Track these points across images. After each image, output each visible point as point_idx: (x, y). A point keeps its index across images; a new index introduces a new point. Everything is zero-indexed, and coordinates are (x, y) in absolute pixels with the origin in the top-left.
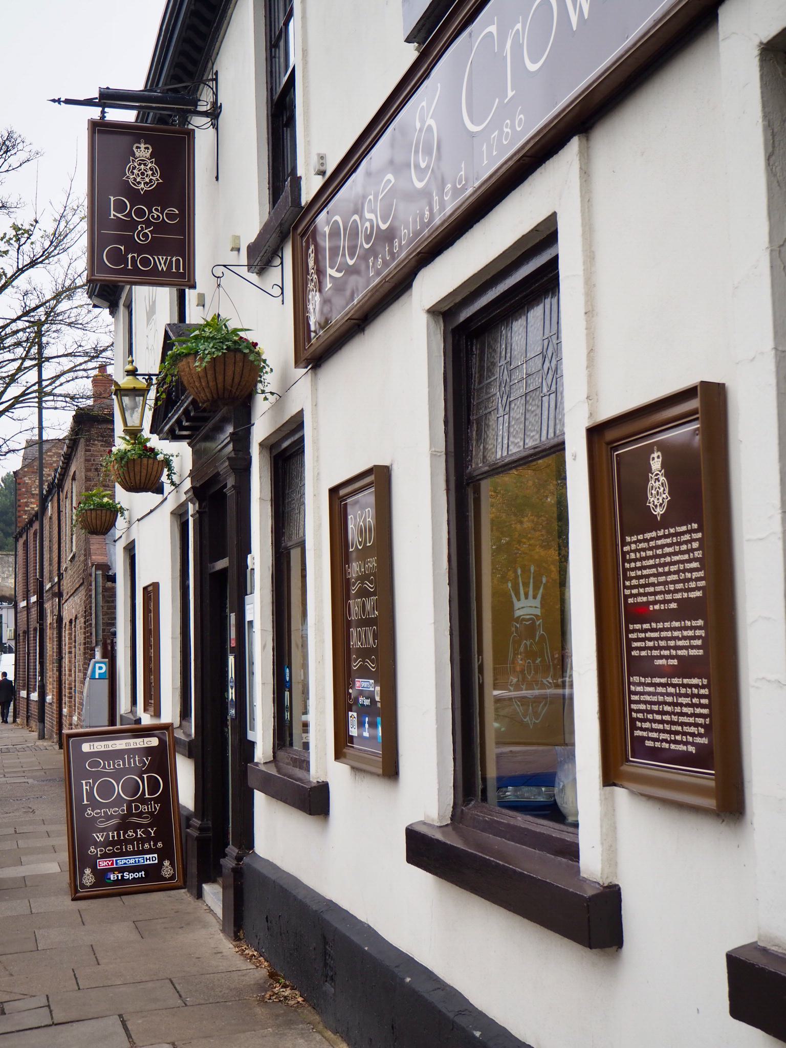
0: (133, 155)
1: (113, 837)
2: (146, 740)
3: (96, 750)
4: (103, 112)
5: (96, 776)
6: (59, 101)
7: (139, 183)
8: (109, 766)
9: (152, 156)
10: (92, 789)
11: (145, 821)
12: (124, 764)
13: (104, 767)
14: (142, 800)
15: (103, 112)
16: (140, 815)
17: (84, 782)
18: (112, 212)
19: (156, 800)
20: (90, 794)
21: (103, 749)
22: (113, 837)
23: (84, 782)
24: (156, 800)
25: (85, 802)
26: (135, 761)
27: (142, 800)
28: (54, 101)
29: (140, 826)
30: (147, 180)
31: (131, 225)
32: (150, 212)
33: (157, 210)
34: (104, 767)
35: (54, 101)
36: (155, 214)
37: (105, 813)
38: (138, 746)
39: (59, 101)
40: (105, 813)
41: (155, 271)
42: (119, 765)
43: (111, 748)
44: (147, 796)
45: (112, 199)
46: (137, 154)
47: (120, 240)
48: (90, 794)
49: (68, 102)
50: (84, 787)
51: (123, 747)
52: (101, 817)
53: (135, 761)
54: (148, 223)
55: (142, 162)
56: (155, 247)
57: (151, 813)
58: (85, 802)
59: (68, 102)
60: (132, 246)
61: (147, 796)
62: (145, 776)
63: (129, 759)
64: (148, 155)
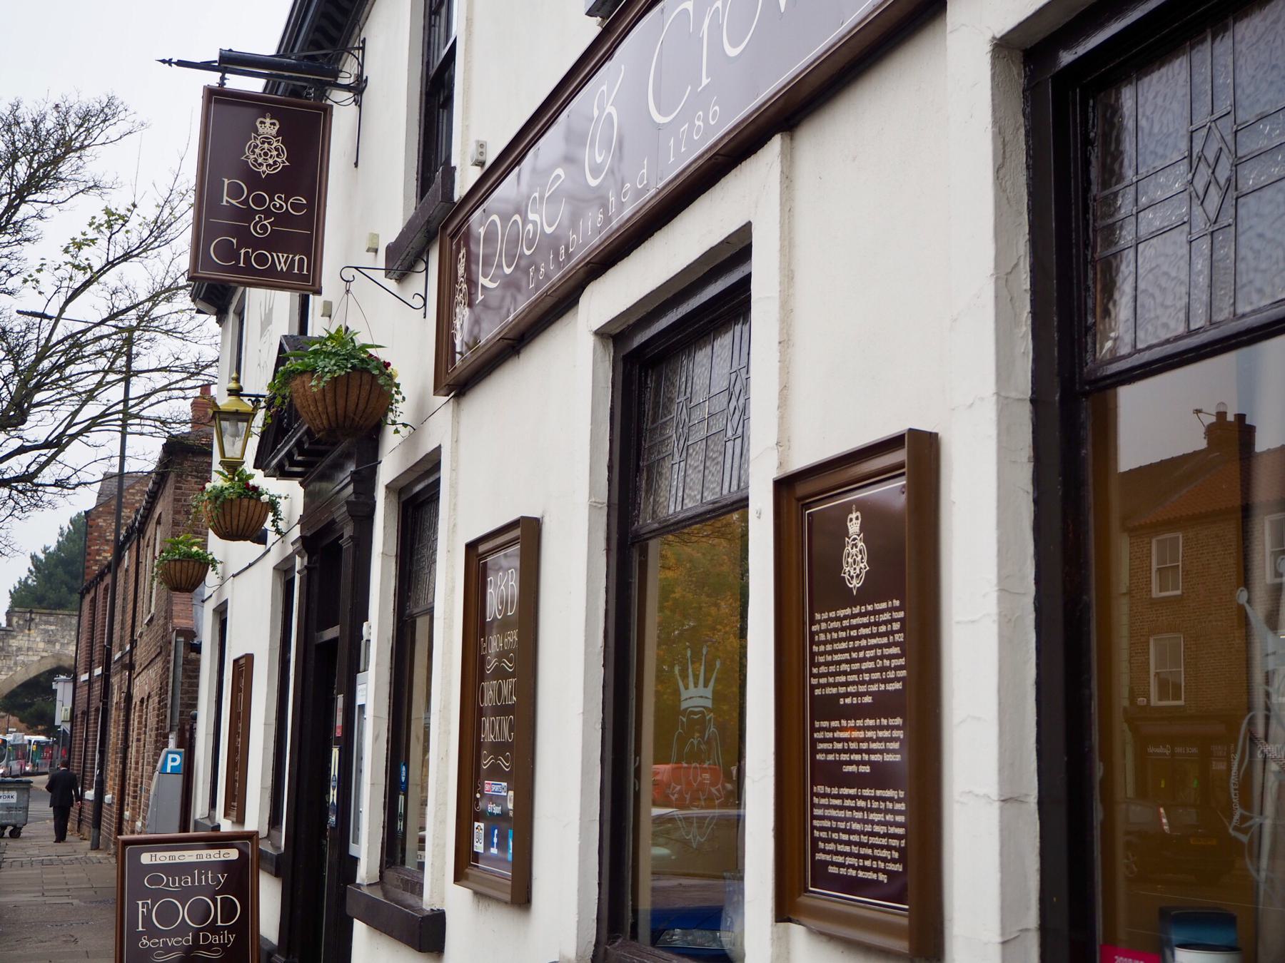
0: (256, 131)
4: (223, 78)
6: (170, 62)
7: (261, 165)
8: (174, 883)
10: (150, 911)
12: (193, 881)
13: (167, 885)
14: (214, 929)
18: (225, 198)
19: (231, 930)
20: (147, 919)
24: (231, 930)
27: (214, 929)
28: (164, 61)
30: (271, 162)
31: (247, 214)
32: (272, 200)
33: (280, 198)
34: (167, 885)
35: (164, 61)
36: (278, 202)
39: (170, 62)
40: (165, 943)
41: (272, 271)
46: (261, 131)
47: (236, 231)
48: (147, 919)
49: (181, 63)
51: (194, 859)
54: (268, 214)
55: (266, 140)
57: (223, 946)
59: (181, 63)
60: (246, 239)
62: (219, 898)
64: (274, 132)
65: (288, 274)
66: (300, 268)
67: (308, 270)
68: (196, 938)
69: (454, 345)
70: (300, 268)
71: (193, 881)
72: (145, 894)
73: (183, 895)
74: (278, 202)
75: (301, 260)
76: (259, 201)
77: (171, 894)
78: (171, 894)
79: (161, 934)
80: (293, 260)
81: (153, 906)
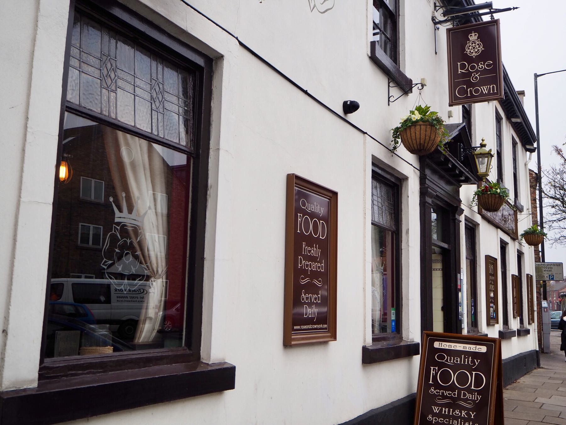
0: (469, 40)
1: (445, 411)
2: (478, 347)
3: (443, 347)
4: (492, 16)
5: (441, 365)
6: (514, 8)
7: (472, 53)
8: (450, 360)
9: (478, 38)
10: (436, 374)
11: (469, 406)
12: (461, 361)
13: (447, 361)
14: (469, 390)
15: (492, 16)
16: (466, 400)
17: (432, 368)
18: (459, 70)
19: (479, 393)
20: (435, 377)
21: (447, 348)
22: (445, 411)
23: (432, 368)
24: (479, 393)
25: (431, 382)
26: (468, 361)
27: (469, 390)
28: (517, 8)
29: (465, 409)
30: (476, 50)
31: (469, 74)
32: (478, 65)
33: (481, 64)
34: (447, 361)
35: (517, 8)
36: (480, 66)
37: (443, 393)
38: (472, 350)
39: (514, 8)
40: (443, 393)
41: (482, 94)
42: (457, 361)
43: (453, 348)
44: (473, 388)
45: (459, 64)
46: (471, 39)
47: (464, 83)
48: (435, 377)
49: (509, 9)
50: (432, 372)
51: (461, 349)
52: (439, 395)
53: (468, 361)
54: (477, 72)
55: (474, 42)
56: (482, 83)
57: (474, 401)
58: (431, 382)
59: (509, 9)
60: (470, 84)
61: (473, 388)
62: (474, 373)
63: (465, 358)
64: (476, 38)
65: (489, 94)
66: (493, 90)
67: (497, 90)
68: (459, 394)
69: (91, 324)
70: (493, 90)
71: (461, 361)
72: (436, 364)
73: (455, 368)
74: (480, 66)
75: (493, 87)
76: (473, 67)
77: (449, 366)
78: (449, 366)
79: (441, 388)
80: (490, 88)
81: (438, 371)
